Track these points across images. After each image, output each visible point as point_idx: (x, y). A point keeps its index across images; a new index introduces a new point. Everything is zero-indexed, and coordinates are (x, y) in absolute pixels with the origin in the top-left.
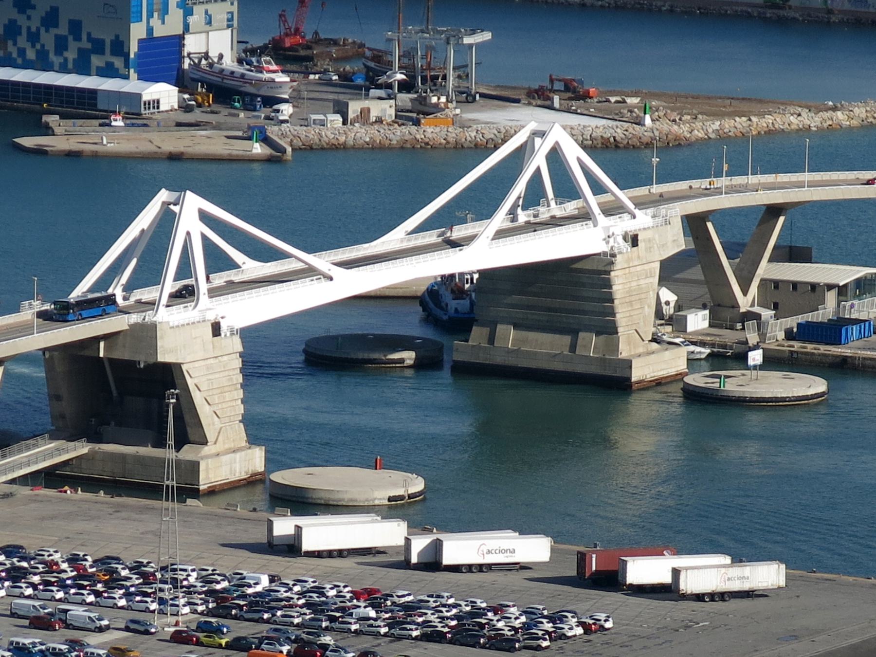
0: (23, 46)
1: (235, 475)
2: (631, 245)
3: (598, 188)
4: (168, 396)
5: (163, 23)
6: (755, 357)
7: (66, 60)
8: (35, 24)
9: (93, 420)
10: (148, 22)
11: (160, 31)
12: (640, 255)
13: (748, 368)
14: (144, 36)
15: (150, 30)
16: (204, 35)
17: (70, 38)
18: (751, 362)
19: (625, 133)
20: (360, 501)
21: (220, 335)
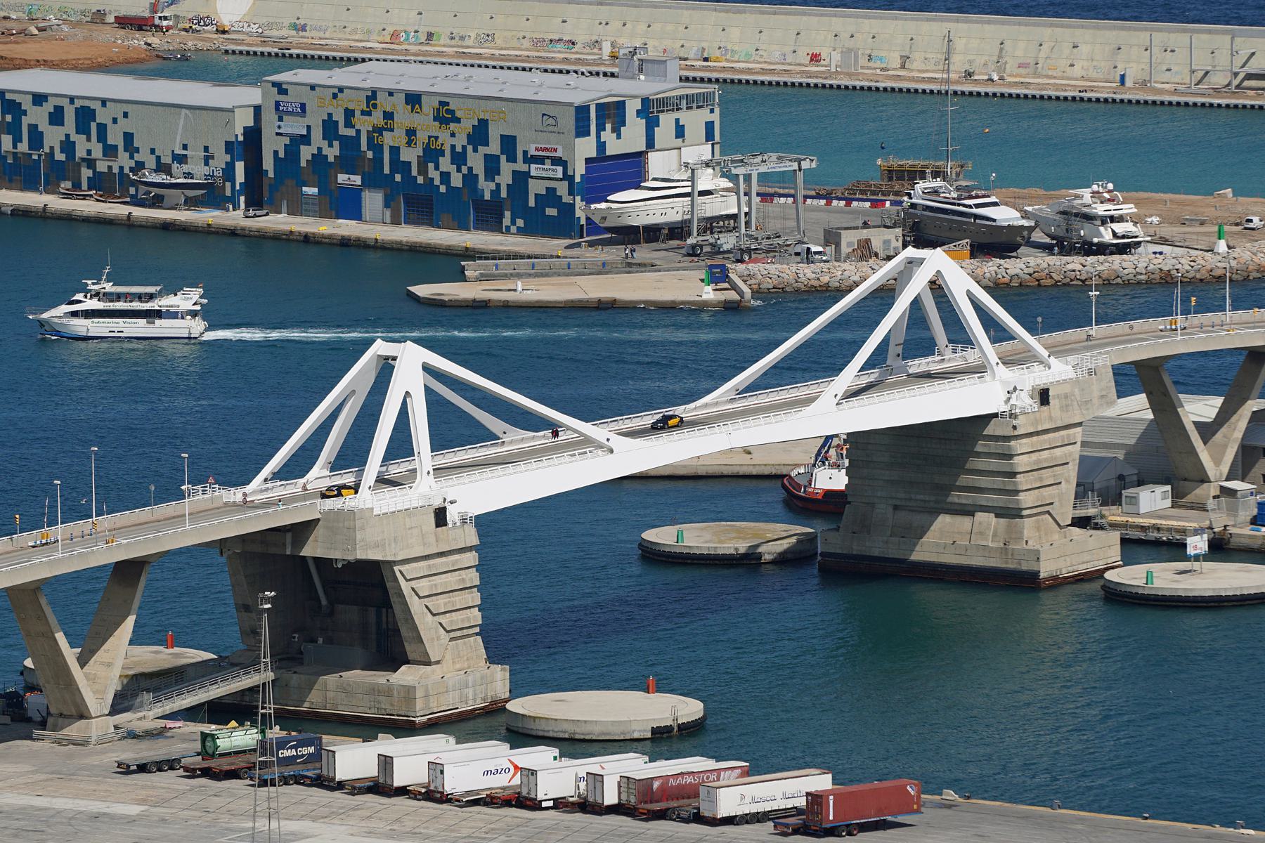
0: (445, 170)
1: (467, 703)
2: (1039, 403)
3: (997, 332)
4: (262, 601)
5: (619, 137)
6: (1197, 544)
7: (498, 185)
8: (461, 141)
9: (297, 636)
10: (598, 136)
11: (614, 147)
12: (1053, 415)
13: (1186, 558)
14: (593, 154)
15: (601, 146)
16: (676, 151)
17: (503, 158)
18: (1191, 551)
19: (1192, 264)
20: (615, 735)
21: (445, 524)
